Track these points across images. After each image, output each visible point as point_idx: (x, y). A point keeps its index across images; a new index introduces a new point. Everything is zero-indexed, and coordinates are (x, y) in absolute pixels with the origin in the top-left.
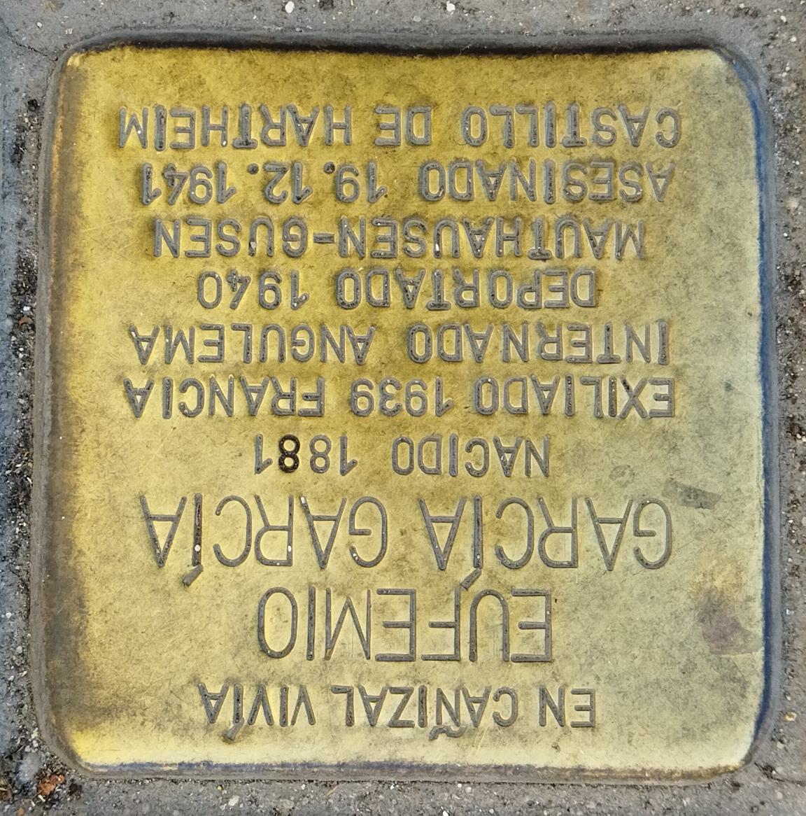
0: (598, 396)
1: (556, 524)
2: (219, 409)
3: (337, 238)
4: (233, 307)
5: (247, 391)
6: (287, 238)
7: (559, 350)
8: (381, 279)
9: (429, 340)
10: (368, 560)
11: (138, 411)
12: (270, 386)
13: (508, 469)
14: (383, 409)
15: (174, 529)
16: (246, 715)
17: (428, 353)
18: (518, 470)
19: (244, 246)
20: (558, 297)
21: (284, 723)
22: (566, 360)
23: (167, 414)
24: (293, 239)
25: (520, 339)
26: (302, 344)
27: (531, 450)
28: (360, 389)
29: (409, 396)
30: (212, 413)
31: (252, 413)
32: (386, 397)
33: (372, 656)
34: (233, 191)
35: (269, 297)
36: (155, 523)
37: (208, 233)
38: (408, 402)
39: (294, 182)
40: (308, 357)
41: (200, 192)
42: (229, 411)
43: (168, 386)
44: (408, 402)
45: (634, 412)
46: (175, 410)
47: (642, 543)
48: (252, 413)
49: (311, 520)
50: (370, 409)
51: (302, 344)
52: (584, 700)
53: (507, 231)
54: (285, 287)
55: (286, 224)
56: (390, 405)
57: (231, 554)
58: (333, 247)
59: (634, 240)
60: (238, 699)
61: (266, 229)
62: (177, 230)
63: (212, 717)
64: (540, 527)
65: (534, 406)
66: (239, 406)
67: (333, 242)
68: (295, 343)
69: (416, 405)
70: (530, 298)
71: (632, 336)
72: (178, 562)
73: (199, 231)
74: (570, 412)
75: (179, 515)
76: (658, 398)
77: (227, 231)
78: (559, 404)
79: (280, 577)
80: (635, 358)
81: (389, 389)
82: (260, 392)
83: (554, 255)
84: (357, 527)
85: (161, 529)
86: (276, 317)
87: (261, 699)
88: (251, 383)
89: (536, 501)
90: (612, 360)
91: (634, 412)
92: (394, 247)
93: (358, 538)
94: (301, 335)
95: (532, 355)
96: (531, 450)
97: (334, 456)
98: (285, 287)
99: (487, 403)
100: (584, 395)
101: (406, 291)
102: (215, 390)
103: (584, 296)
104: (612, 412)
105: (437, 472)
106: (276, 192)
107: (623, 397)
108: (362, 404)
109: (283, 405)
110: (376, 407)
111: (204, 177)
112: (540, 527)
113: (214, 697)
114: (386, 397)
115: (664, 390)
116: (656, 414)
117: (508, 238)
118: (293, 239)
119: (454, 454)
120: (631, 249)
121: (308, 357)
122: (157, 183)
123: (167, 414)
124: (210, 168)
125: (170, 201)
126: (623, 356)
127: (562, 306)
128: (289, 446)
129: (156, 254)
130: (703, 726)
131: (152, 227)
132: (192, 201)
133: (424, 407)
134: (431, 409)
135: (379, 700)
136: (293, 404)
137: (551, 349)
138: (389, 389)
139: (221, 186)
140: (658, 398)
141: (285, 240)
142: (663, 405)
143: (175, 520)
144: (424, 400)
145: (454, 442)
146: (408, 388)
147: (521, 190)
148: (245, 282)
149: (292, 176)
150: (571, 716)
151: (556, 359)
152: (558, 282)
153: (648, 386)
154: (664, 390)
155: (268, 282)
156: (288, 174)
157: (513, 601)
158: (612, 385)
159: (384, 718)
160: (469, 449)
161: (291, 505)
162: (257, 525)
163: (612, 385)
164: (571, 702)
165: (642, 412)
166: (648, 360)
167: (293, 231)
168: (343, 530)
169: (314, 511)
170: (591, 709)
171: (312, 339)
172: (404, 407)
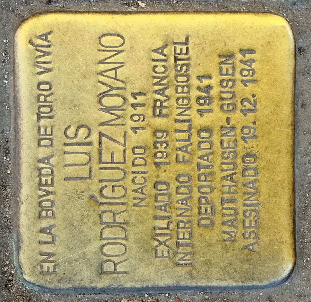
0: (163, 228)
1: (117, 217)
3: (228, 126)
5: (164, 90)
6: (228, 105)
7: (181, 228)
8: (209, 147)
11: (154, 51)
13: (136, 191)
14: (158, 142)
17: (180, 182)
18: (136, 195)
19: (225, 161)
21: (38, 62)
22: (178, 231)
23: (154, 60)
24: (228, 108)
25: (185, 214)
26: (183, 102)
28: (165, 134)
30: (154, 77)
31: (155, 92)
32: (161, 143)
34: (246, 86)
35: (202, 101)
36: (114, 71)
37: (229, 75)
38: (160, 152)
41: (245, 73)
42: (155, 84)
44: (160, 152)
45: (157, 243)
48: (155, 92)
49: (115, 69)
50: (157, 138)
51: (183, 102)
54: (206, 107)
56: (158, 145)
58: (225, 124)
59: (229, 238)
60: (49, 46)
62: (230, 64)
63: (40, 37)
66: (157, 88)
67: (227, 125)
69: (159, 155)
70: (203, 201)
71: (186, 254)
74: (156, 218)
75: (118, 80)
76: (162, 252)
77: (230, 84)
78: (160, 213)
80: (178, 110)
82: (163, 94)
83: (223, 206)
87: (46, 54)
94: (185, 90)
95: (181, 218)
98: (206, 107)
100: (162, 223)
101: (205, 157)
102: (163, 78)
103: (203, 222)
105: (134, 165)
108: (159, 134)
109: (158, 104)
110: (158, 140)
112: (116, 259)
113: (46, 38)
114: (161, 143)
115: (166, 254)
119: (138, 173)
120: (226, 236)
123: (154, 60)
124: (255, 134)
127: (200, 213)
129: (220, 56)
131: (230, 56)
132: (242, 70)
133: (158, 158)
134: (157, 161)
135: (49, 233)
136: (158, 107)
137: (181, 225)
139: (248, 138)
140: (162, 252)
142: (160, 254)
143: (115, 78)
144: (161, 158)
145: (145, 172)
146: (165, 152)
147: (247, 196)
148: (207, 92)
151: (178, 227)
152: (209, 210)
153: (167, 248)
154: (166, 254)
157: (87, 167)
160: (143, 177)
165: (157, 246)
167: (231, 107)
171: (185, 105)
172: (158, 150)
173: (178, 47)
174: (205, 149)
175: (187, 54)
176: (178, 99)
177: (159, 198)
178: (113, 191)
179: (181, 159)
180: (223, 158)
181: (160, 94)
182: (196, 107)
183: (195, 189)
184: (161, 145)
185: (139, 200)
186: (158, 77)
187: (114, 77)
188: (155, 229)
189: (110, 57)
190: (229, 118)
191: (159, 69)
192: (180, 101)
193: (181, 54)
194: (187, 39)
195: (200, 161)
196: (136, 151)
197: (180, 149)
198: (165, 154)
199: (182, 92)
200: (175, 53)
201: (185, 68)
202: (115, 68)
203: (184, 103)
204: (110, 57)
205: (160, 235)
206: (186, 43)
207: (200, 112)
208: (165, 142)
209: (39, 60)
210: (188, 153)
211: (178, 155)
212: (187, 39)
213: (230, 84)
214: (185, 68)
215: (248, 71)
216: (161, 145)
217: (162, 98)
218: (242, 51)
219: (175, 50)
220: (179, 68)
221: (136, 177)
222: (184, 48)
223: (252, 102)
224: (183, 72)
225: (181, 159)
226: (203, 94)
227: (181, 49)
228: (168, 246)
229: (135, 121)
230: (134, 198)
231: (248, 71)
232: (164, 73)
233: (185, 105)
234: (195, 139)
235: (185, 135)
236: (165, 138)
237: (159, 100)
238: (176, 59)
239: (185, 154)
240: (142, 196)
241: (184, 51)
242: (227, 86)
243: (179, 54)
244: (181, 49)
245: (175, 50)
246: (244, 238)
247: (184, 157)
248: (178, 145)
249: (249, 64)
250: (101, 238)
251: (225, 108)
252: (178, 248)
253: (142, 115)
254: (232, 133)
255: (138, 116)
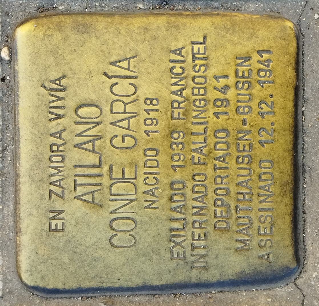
2: (174, 81)
4: (215, 88)
6: (244, 107)
9: (201, 84)
10: (113, 90)
12: (63, 142)
15: (125, 69)
16: (52, 93)
19: (239, 92)
20: (219, 214)
21: (51, 108)
23: (171, 61)
24: (244, 110)
26: (200, 103)
27: (154, 202)
29: (179, 155)
30: (172, 78)
31: (173, 93)
33: (77, 178)
39: (267, 113)
40: (195, 105)
41: (262, 73)
43: (183, 62)
45: (173, 244)
46: (172, 65)
47: (120, 138)
48: (173, 93)
49: (128, 119)
51: (200, 103)
52: (60, 228)
53: (247, 197)
55: (250, 108)
57: (115, 89)
60: (60, 90)
61: (249, 173)
64: (126, 100)
65: (174, 205)
68: (200, 100)
69: (176, 158)
70: (219, 203)
72: (113, 70)
73: (246, 74)
74: (172, 220)
79: (107, 109)
81: (180, 146)
84: (126, 138)
85: (124, 64)
86: (210, 106)
87: (60, 99)
88: (184, 92)
89: (136, 98)
90: (193, 247)
91: (173, 244)
92: (240, 77)
93: (121, 138)
96: (154, 202)
97: (152, 128)
99: (176, 186)
104: (174, 236)
106: (263, 105)
107: (179, 240)
108: (175, 135)
109: (176, 105)
110: (176, 141)
111: (268, 75)
112: (125, 99)
116: (171, 252)
117: (244, 197)
118: (244, 110)
121: (195, 105)
122: (266, 56)
123: (171, 61)
125: (259, 62)
126: (194, 253)
128: (155, 102)
130: (47, 154)
132: (259, 71)
135: (59, 186)
138: (180, 146)
141: (244, 163)
144: (264, 77)
146: (182, 155)
147: (262, 198)
149: (270, 112)
150: (54, 222)
155: (224, 103)
156: (270, 110)
158: (184, 236)
159: (52, 188)
160: (154, 178)
161: (134, 113)
162: (126, 100)
163: (184, 236)
164: (59, 222)
166: (194, 117)
168: (126, 132)
169: (131, 120)
170: (56, 230)
171: (202, 107)
172: (176, 152)
173: (196, 47)
174: (222, 150)
175: (204, 53)
176: (195, 101)
177: (176, 198)
178: (123, 141)
179: (196, 161)
180: (237, 163)
181: (177, 95)
182: (212, 110)
183: (210, 190)
184: (178, 146)
185: (151, 203)
186: (178, 78)
187: (127, 67)
188: (172, 230)
189: (124, 206)
190: (245, 119)
191: (178, 70)
192: (197, 103)
193: (198, 53)
194: (205, 37)
195: (216, 162)
196: (148, 153)
197: (194, 150)
198: (183, 156)
199: (199, 94)
200: (193, 53)
201: (203, 68)
202: (128, 58)
203: (201, 105)
204: (124, 206)
205: (180, 236)
206: (204, 43)
207: (217, 115)
208: (181, 143)
209: (52, 105)
210: (203, 154)
211: (193, 157)
212: (205, 37)
213: (246, 86)
214: (203, 68)
215: (266, 71)
216: (178, 146)
217: (59, 142)
218: (260, 53)
219: (193, 49)
220: (197, 68)
221: (148, 177)
222: (201, 47)
223: (270, 104)
224: (200, 74)
225: (196, 161)
226: (221, 96)
227: (199, 49)
228: (183, 247)
229: (148, 125)
230: (145, 201)
231: (266, 71)
232: (182, 73)
233: (202, 107)
234: (211, 141)
235: (201, 139)
236: (183, 138)
237: (177, 101)
238: (194, 59)
239: (199, 155)
240: (153, 198)
241: (202, 51)
242: (242, 88)
243: (197, 54)
244: (199, 49)
245: (193, 49)
246: (260, 247)
247: (199, 159)
248: (194, 147)
249: (266, 64)
250: (111, 194)
251: (241, 110)
252: (193, 250)
253: (155, 119)
254: (247, 63)
255: (178, 133)
